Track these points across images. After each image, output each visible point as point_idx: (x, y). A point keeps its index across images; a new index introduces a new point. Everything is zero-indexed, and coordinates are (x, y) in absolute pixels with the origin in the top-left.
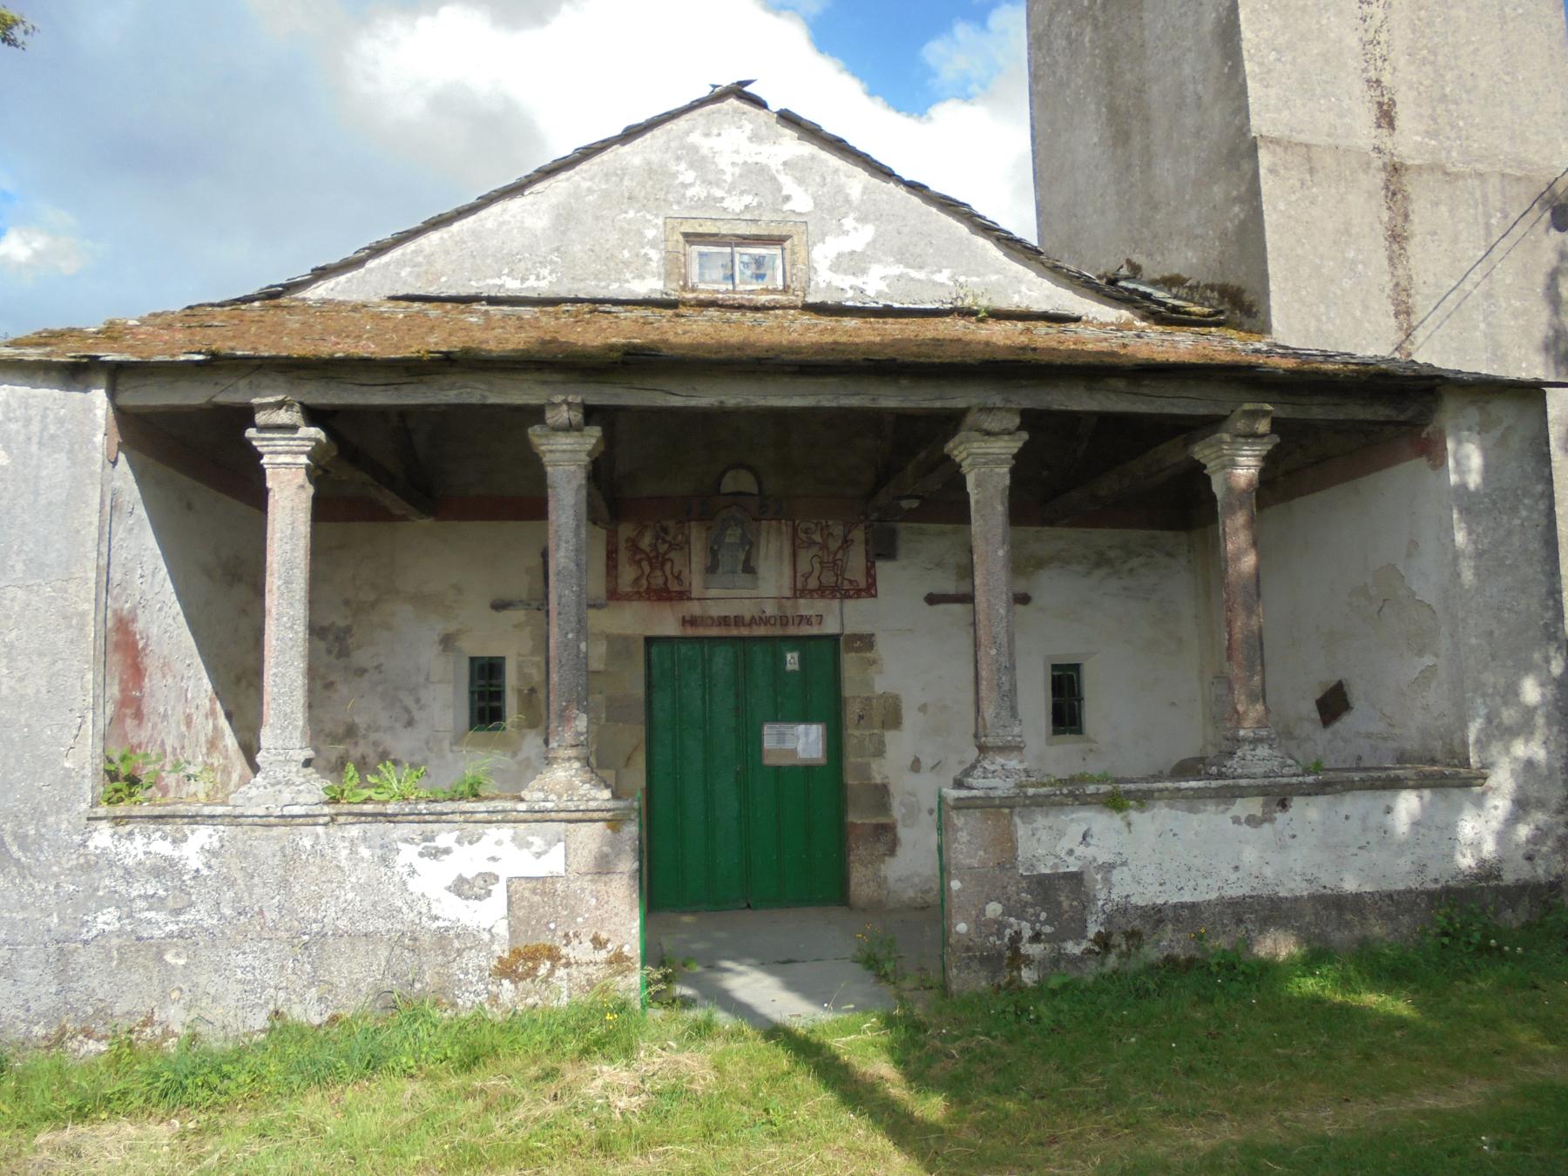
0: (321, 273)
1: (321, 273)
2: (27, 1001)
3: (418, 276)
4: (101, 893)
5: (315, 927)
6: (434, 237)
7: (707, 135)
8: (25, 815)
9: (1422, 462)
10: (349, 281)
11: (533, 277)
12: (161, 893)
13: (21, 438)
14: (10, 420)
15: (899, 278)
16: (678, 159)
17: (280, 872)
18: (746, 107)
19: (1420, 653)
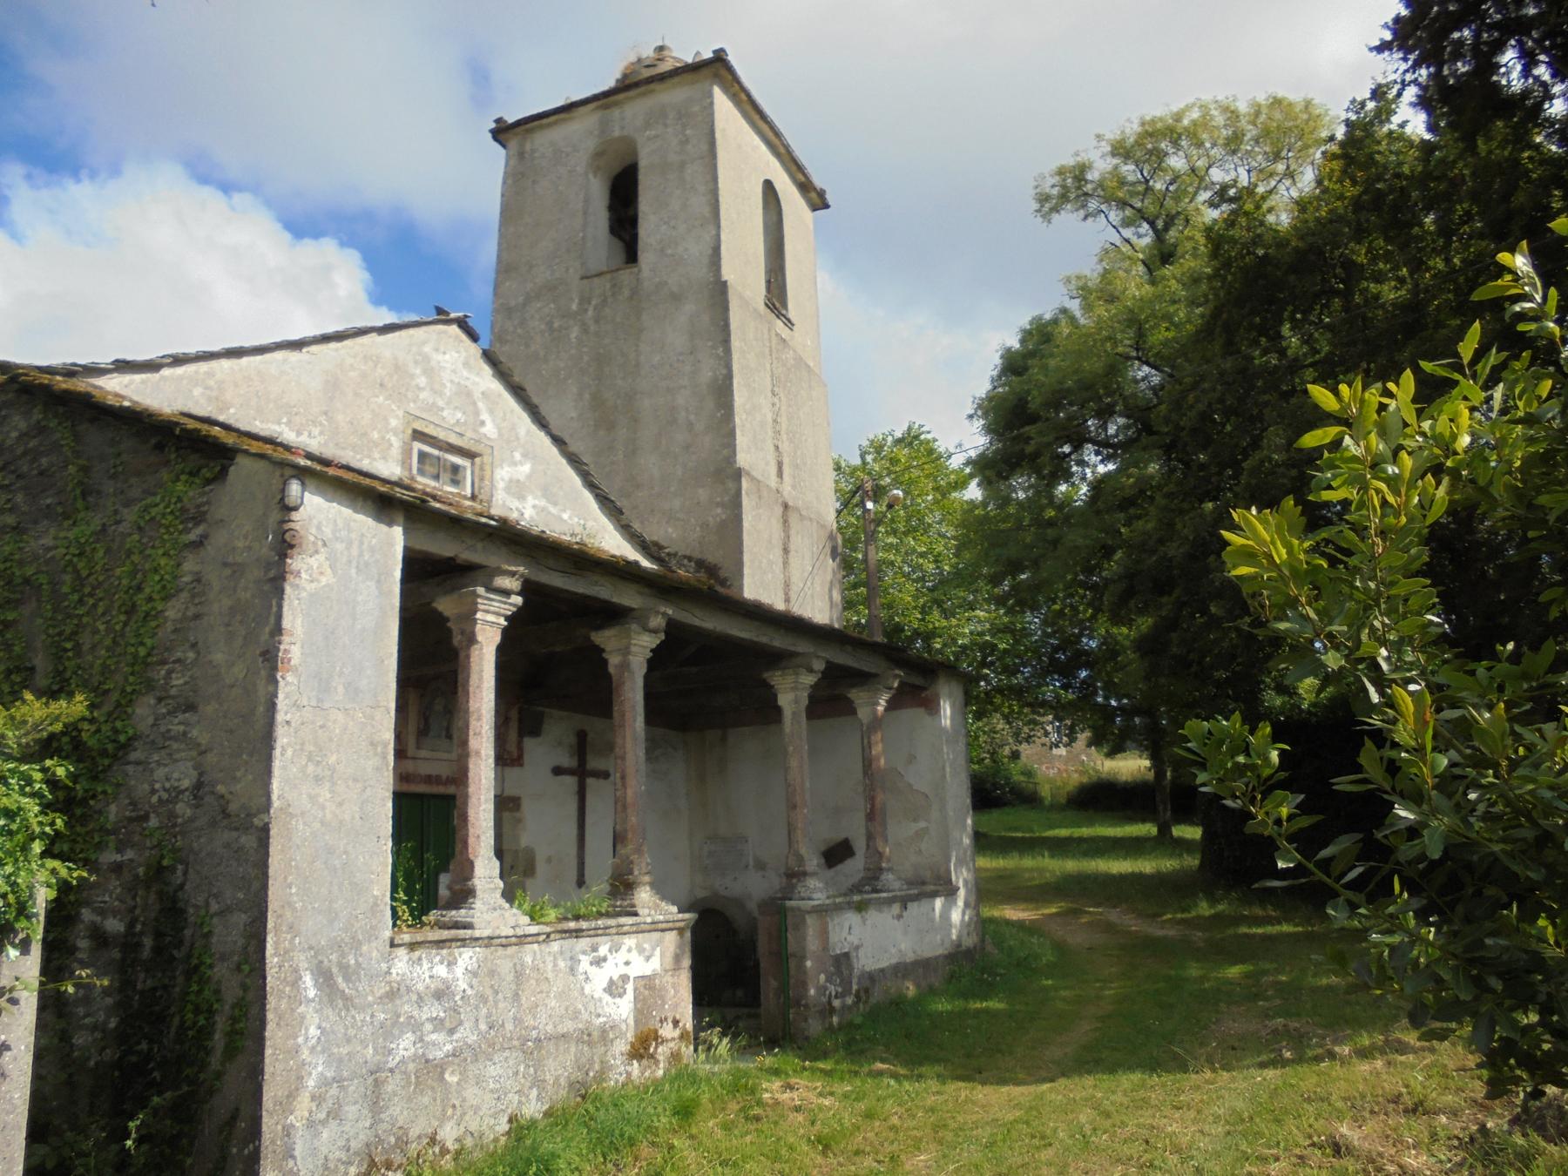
0: (123, 366)
1: (123, 366)
2: (348, 1140)
3: (209, 399)
4: (402, 1020)
5: (534, 1033)
6: (225, 363)
7: (437, 350)
8: (346, 944)
9: (920, 711)
10: (143, 382)
11: (306, 433)
12: (442, 1014)
13: (344, 560)
14: (337, 539)
15: (543, 509)
16: (416, 362)
17: (514, 987)
18: (464, 337)
19: (915, 820)
